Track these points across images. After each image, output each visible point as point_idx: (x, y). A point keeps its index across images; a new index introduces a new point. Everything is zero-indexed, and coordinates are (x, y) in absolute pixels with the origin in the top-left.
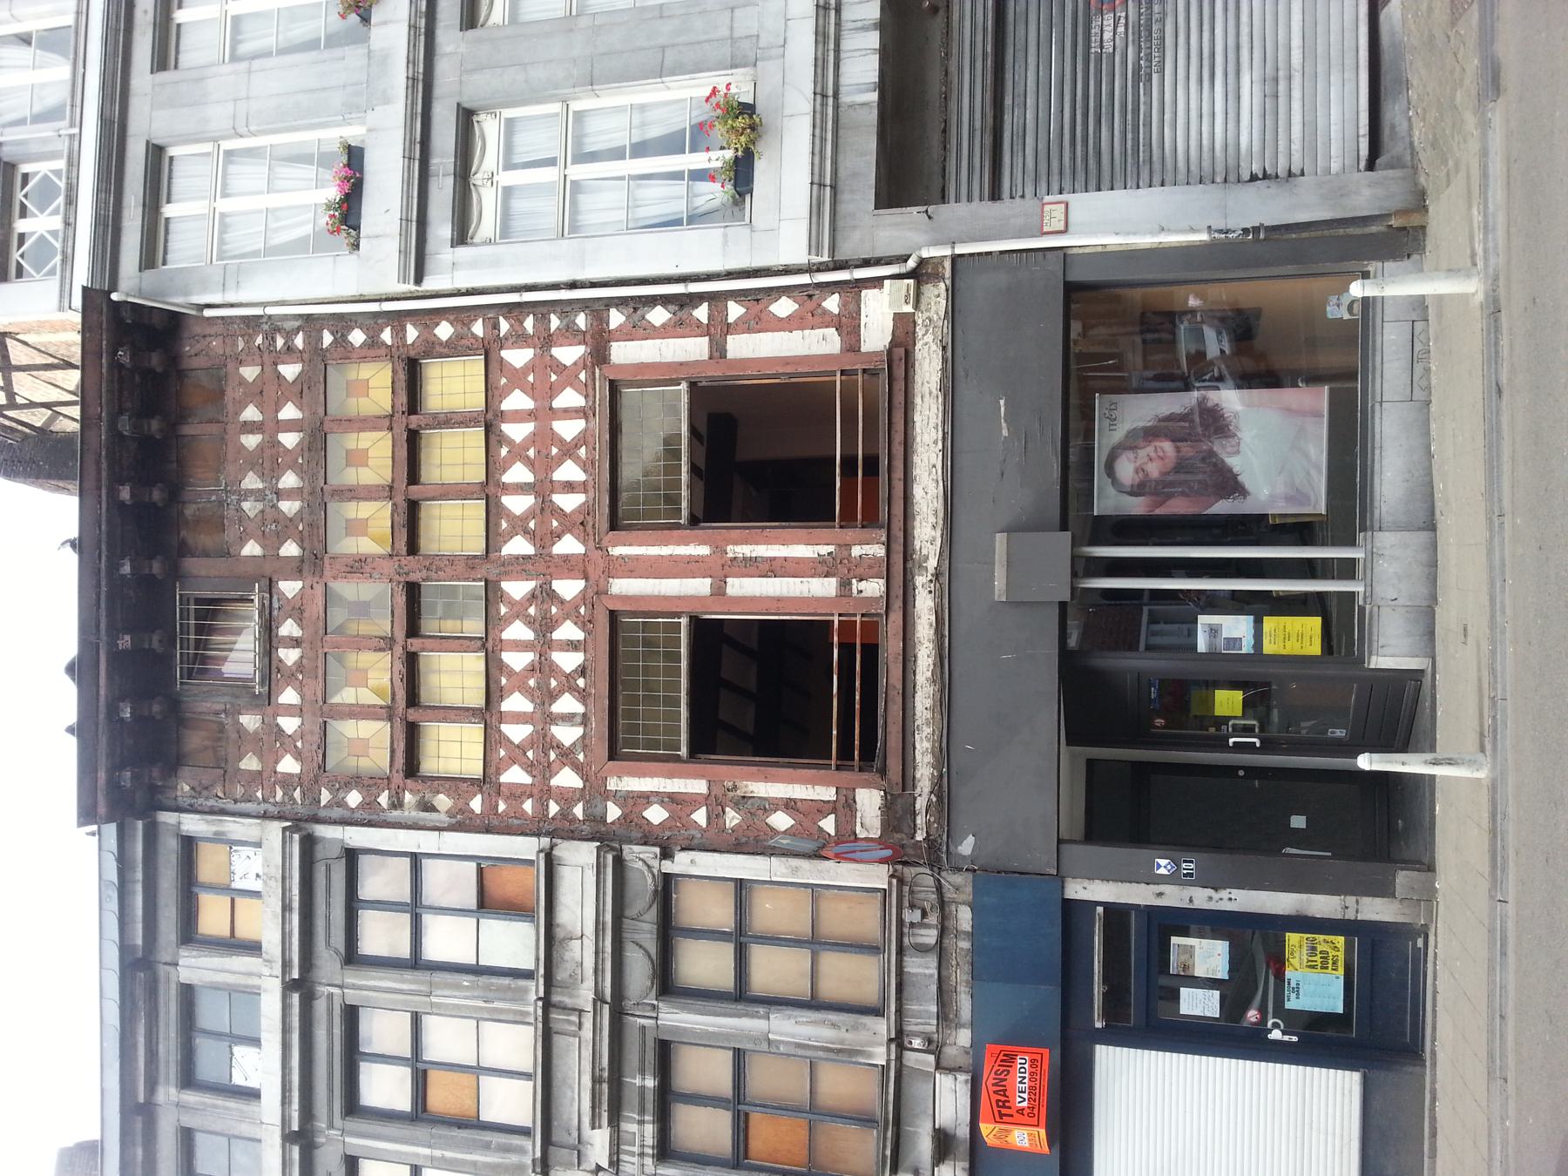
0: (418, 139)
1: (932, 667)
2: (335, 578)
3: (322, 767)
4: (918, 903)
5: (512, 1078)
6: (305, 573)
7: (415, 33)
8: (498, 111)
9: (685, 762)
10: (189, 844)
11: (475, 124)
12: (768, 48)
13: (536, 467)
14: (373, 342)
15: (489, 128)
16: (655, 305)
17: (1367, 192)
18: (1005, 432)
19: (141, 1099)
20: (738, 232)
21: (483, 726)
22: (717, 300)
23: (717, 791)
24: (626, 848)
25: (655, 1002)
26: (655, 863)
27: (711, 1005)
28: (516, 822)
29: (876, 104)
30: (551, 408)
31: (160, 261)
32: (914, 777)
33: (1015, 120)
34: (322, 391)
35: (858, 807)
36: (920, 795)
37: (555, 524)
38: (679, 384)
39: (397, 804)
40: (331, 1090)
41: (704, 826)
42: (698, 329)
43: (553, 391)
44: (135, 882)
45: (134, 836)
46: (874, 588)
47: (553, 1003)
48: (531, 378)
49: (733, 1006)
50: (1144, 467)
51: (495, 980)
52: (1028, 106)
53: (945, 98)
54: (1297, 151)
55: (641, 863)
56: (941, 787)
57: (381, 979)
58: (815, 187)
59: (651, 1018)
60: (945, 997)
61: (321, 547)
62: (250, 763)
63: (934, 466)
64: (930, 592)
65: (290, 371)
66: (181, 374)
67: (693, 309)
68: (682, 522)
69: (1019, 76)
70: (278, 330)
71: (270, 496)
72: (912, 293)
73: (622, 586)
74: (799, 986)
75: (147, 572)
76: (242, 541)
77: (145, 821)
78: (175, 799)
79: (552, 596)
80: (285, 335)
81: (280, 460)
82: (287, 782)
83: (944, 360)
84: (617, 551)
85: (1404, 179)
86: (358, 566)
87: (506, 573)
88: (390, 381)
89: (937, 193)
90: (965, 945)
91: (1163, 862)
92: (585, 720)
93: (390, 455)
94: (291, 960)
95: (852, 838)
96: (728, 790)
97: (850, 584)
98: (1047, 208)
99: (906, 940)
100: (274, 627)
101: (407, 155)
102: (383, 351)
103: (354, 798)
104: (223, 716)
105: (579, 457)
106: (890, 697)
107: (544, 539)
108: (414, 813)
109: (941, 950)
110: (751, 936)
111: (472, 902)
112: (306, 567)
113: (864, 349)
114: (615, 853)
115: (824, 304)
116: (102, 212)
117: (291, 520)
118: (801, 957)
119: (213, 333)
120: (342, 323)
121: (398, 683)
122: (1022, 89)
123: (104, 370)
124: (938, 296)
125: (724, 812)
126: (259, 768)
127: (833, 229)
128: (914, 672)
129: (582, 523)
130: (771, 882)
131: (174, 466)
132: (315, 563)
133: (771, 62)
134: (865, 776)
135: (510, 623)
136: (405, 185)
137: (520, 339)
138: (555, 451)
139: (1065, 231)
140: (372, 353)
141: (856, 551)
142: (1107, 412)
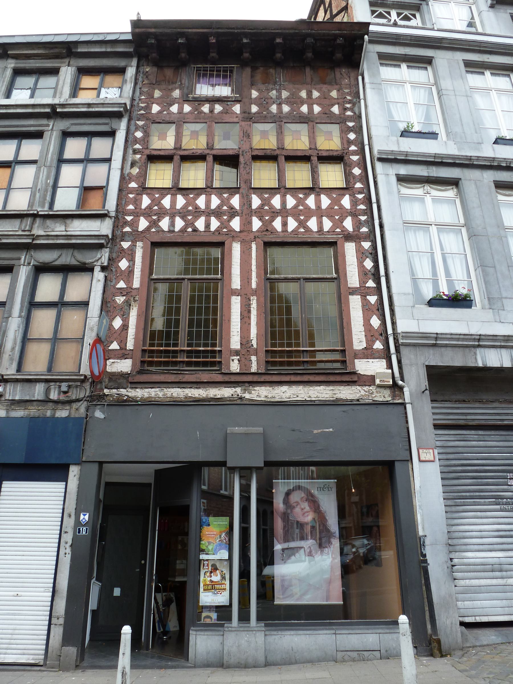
1: (194, 396)
2: (241, 126)
3: (154, 122)
5: (4, 203)
6: (243, 115)
7: (491, 160)
8: (458, 197)
9: (149, 277)
11: (452, 187)
12: (499, 315)
13: (294, 210)
14: (350, 142)
15: (450, 193)
16: (373, 262)
18: (315, 432)
19: (9, 52)
21: (171, 187)
23: (134, 293)
25: (32, 264)
26: (99, 263)
27: (28, 290)
28: (123, 202)
29: (476, 365)
30: (322, 216)
32: (137, 388)
33: (472, 436)
34: (327, 122)
35: (123, 361)
36: (127, 391)
37: (267, 218)
38: (336, 274)
39: (135, 152)
42: (363, 281)
43: (331, 217)
44: (106, 48)
45: (127, 48)
46: (235, 366)
48: (336, 207)
49: (27, 300)
52: (479, 442)
53: (480, 401)
54: (465, 583)
55: (100, 256)
56: (131, 401)
57: (54, 146)
58: (435, 335)
59: (24, 262)
60: (23, 404)
61: (256, 121)
62: (157, 94)
63: (297, 396)
64: (232, 395)
65: (335, 109)
66: (332, 68)
67: (372, 280)
70: (354, 104)
71: (278, 101)
72: (386, 383)
73: (236, 249)
74: (35, 332)
75: (244, 51)
76: (258, 90)
78: (143, 66)
79: (232, 216)
80: (352, 107)
81: (295, 105)
82: (148, 108)
83: (352, 400)
84: (254, 246)
85: (457, 643)
86: (247, 135)
88: (333, 149)
89: (435, 398)
90: (49, 413)
91: (87, 517)
94: (65, 108)
95: (107, 358)
96: (134, 298)
97: (237, 355)
98: (431, 451)
101: (436, 155)
102: (346, 146)
103: (139, 134)
104: (179, 83)
105: (299, 228)
106: (178, 375)
107: (259, 213)
108: (130, 159)
109: (47, 401)
110: (61, 309)
111: (86, 184)
112: (246, 115)
113: (356, 360)
115: (378, 342)
116: (402, 38)
117: (268, 109)
118: (48, 334)
120: (358, 130)
123: (333, 32)
125: (123, 296)
127: (414, 345)
128: (191, 388)
129: (267, 230)
130: (86, 318)
131: (292, 65)
132: (248, 118)
133: (492, 316)
134: (139, 364)
135: (219, 198)
137: (354, 202)
138: (302, 218)
139: (420, 461)
140: (345, 142)
141: (254, 358)
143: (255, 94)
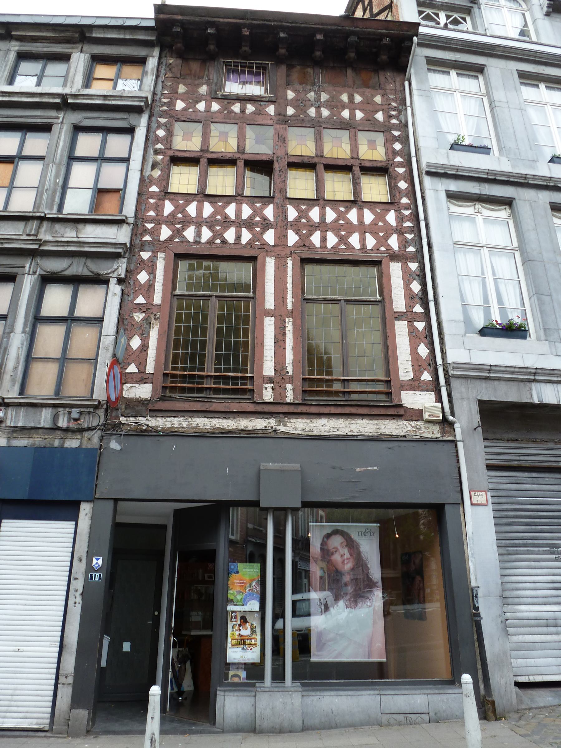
0: (497, 178)
1: (222, 427)
3: (178, 120)
4: (83, 417)
6: (278, 117)
7: (547, 180)
9: (172, 293)
10: (142, 61)
11: (504, 207)
13: (334, 224)
14: (395, 153)
16: (421, 285)
17: (503, 682)
18: (358, 470)
19: (13, 33)
20: (461, 328)
22: (426, 316)
23: (154, 309)
24: (125, 260)
25: (38, 273)
26: (115, 275)
28: (143, 208)
30: (365, 232)
31: (429, 67)
32: (158, 417)
33: (525, 479)
34: (370, 129)
35: (142, 385)
36: (147, 420)
37: (304, 232)
38: (380, 296)
39: (157, 152)
40: (8, 116)
41: (135, 302)
42: (410, 306)
43: (374, 234)
44: (125, 34)
45: (148, 35)
46: (268, 395)
47: (43, 222)
48: (380, 223)
50: (337, 552)
51: (58, 195)
53: (534, 441)
55: (116, 267)
56: (151, 431)
58: (488, 367)
60: (26, 431)
62: (182, 89)
63: (338, 430)
64: (266, 427)
65: (380, 116)
66: (376, 71)
67: (420, 304)
68: (305, 295)
69: (548, 481)
70: (400, 112)
72: (435, 418)
73: (270, 264)
74: (40, 351)
76: (294, 91)
77: (155, 42)
78: (166, 57)
80: (397, 115)
81: (335, 109)
82: (171, 104)
83: (398, 436)
84: (290, 262)
86: (282, 140)
87: (278, 207)
90: (57, 443)
91: (100, 562)
92: (197, 242)
93: (339, 157)
94: (78, 99)
95: (123, 381)
96: (155, 315)
97: (271, 383)
98: (484, 494)
99: (61, 409)
100: (251, 102)
101: (489, 171)
102: (391, 157)
104: (207, 79)
105: (340, 245)
107: (296, 226)
109: (55, 429)
110: (70, 326)
111: (100, 186)
112: (281, 117)
114: (123, 253)
115: (426, 372)
116: (452, 42)
117: (305, 112)
119: (396, 85)
120: (405, 140)
121: (220, 155)
122: (541, 483)
123: (380, 31)
124: (433, 434)
125: (142, 312)
126: (179, 92)
129: (304, 245)
131: (332, 65)
132: (283, 121)
133: (548, 348)
134: (160, 389)
135: (251, 208)
136: (475, 170)
137: (400, 219)
138: (343, 233)
139: (472, 504)
140: (390, 152)
141: (289, 387)
142: (369, 530)
143: (291, 95)
